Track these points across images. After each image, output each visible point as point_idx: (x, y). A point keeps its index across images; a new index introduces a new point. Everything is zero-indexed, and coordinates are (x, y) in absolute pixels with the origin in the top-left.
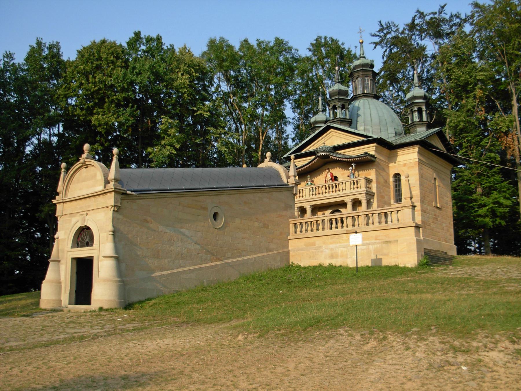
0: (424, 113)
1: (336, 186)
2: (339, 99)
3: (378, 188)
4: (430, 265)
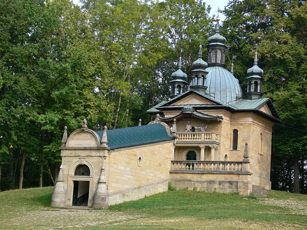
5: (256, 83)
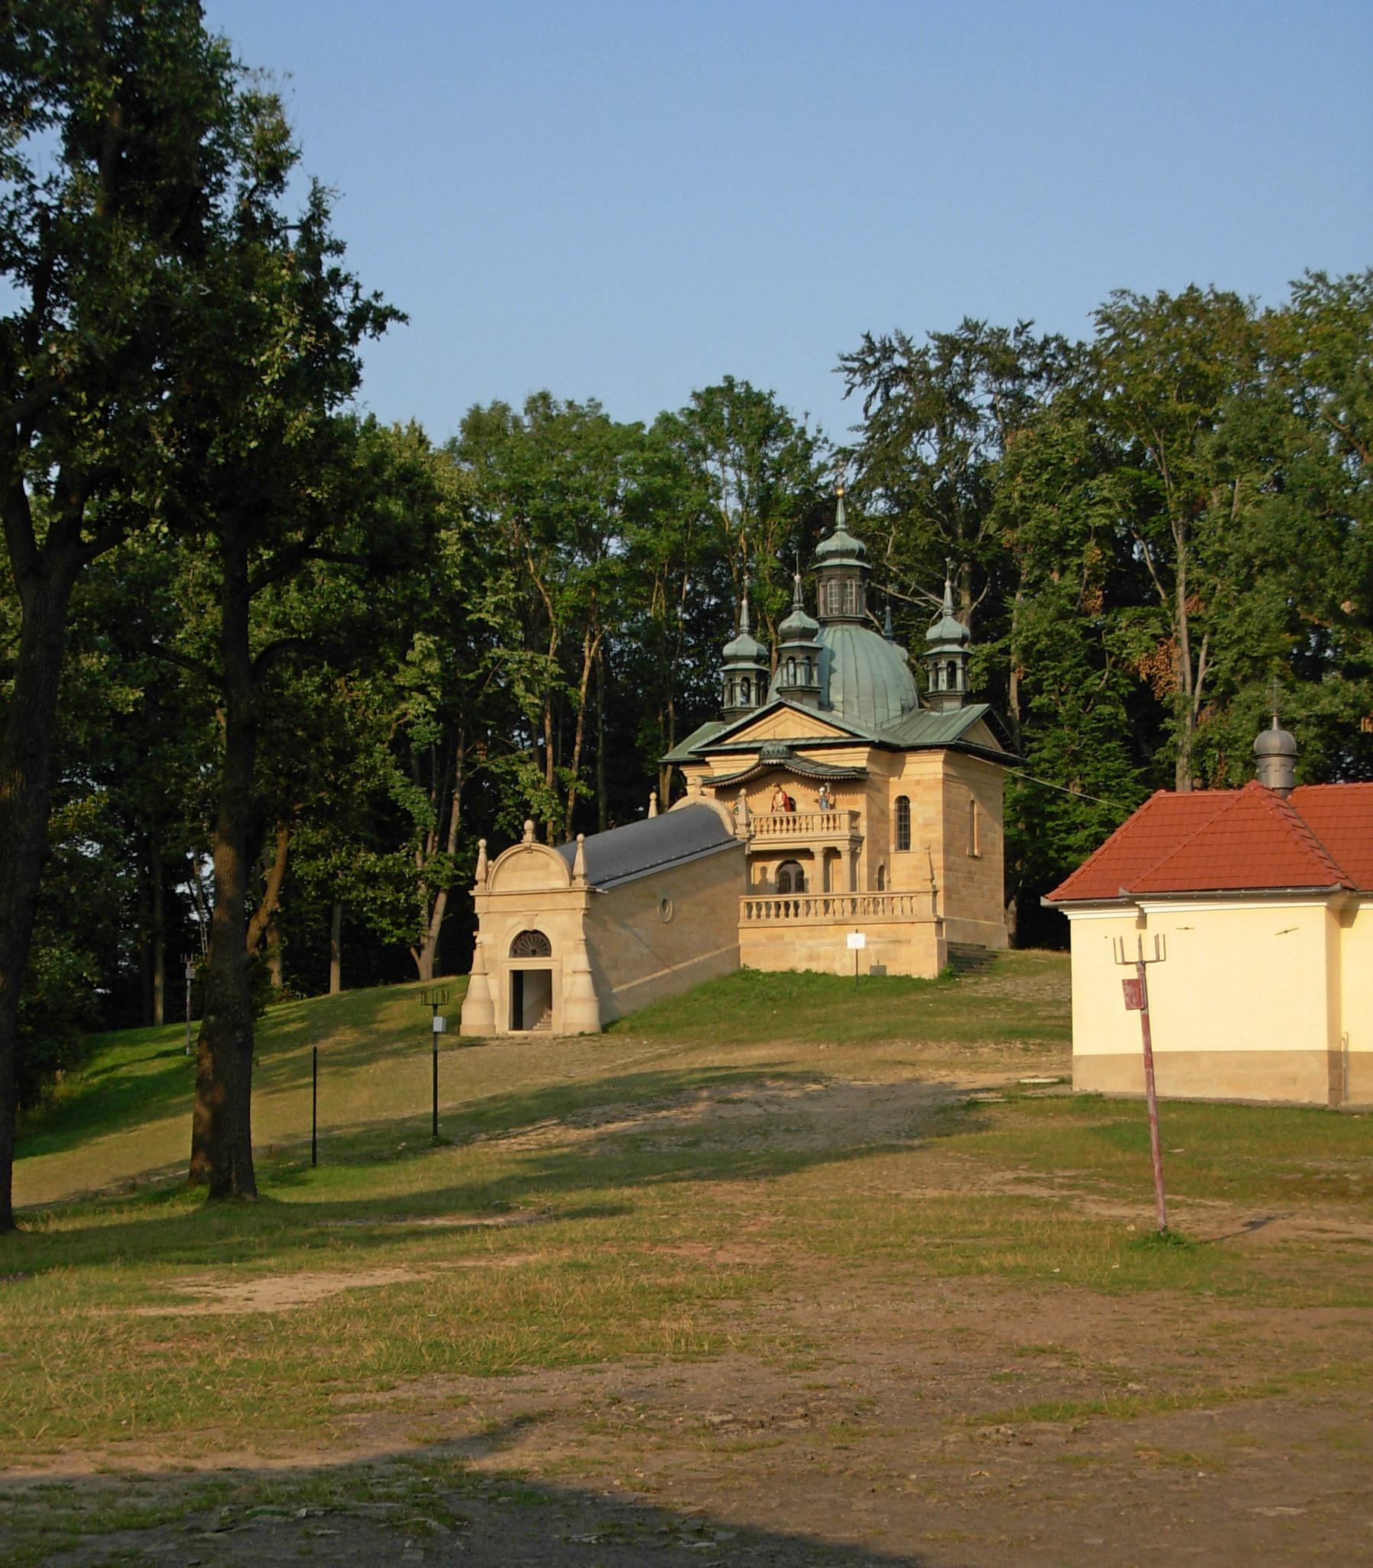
0: (959, 674)
1: (795, 821)
2: (802, 647)
3: (869, 827)
4: (955, 976)
5: (952, 666)
